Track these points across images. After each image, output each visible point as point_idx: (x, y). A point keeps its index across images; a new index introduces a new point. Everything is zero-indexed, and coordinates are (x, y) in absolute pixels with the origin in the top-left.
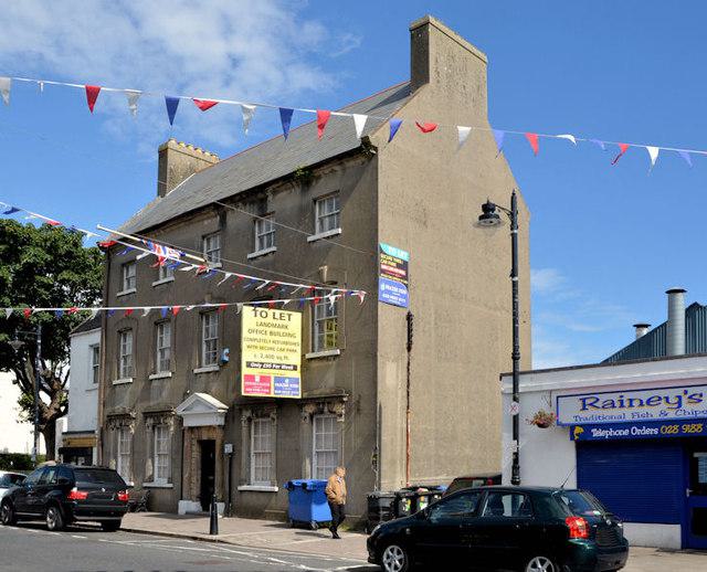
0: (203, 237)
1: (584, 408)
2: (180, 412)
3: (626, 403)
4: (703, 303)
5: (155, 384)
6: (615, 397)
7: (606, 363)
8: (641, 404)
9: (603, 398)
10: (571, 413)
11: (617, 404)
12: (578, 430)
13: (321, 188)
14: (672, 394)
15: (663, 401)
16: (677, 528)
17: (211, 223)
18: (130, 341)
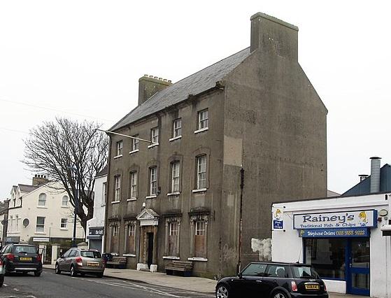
0: (152, 129)
1: (305, 221)
2: (138, 219)
3: (322, 219)
4: (390, 164)
5: (129, 203)
6: (318, 216)
7: (343, 196)
8: (328, 220)
9: (312, 216)
10: (300, 222)
11: (318, 220)
12: (302, 232)
13: (201, 106)
14: (341, 215)
15: (337, 219)
16: (344, 283)
17: (155, 122)
18: (178, 169)
